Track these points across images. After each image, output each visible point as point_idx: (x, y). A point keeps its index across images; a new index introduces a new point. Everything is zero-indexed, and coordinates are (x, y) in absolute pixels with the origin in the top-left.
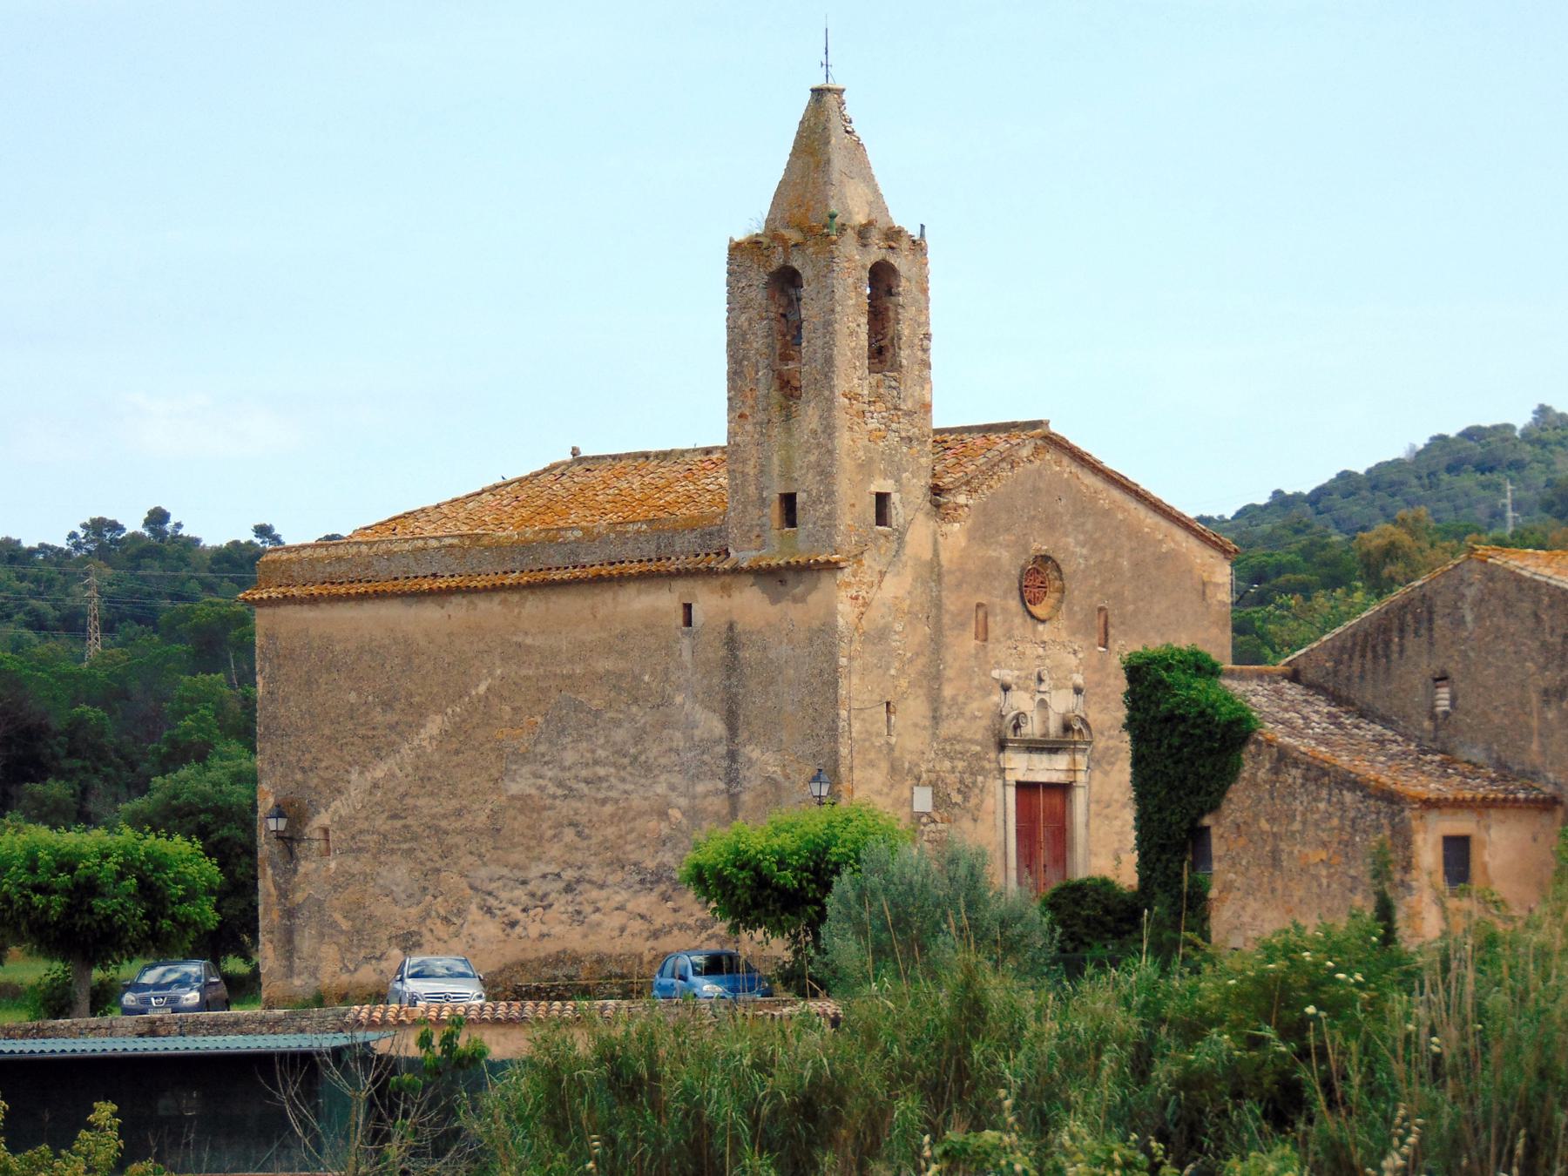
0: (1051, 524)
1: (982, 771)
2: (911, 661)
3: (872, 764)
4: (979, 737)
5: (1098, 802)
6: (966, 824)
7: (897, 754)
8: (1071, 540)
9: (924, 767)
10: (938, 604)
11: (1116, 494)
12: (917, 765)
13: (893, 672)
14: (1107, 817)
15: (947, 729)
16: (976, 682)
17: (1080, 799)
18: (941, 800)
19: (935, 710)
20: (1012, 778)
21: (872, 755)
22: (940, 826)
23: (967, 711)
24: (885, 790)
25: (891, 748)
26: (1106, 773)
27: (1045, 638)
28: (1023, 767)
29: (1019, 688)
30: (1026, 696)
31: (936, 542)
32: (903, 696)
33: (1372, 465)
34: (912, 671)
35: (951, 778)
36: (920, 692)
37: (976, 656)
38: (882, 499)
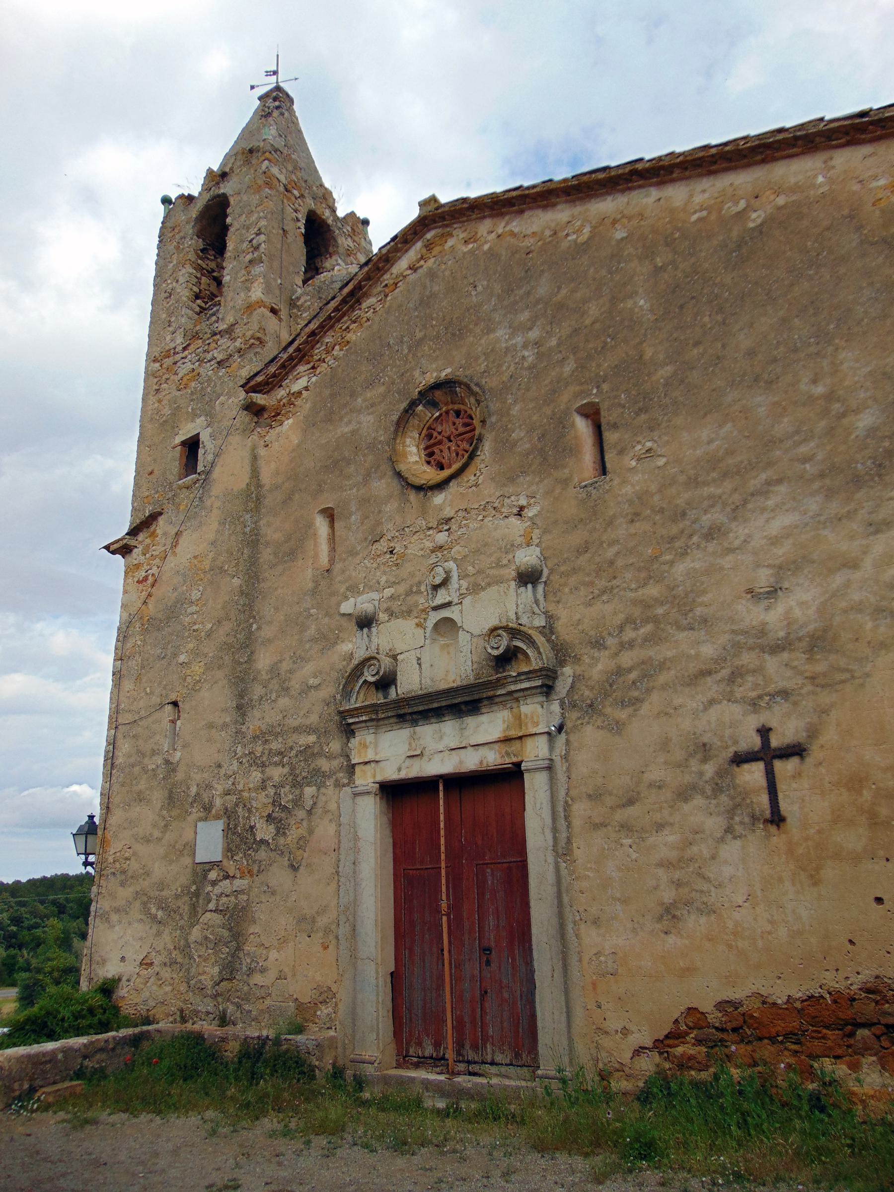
0: (455, 332)
1: (318, 777)
2: (209, 635)
3: (140, 798)
4: (314, 719)
5: (595, 797)
6: (279, 876)
7: (180, 776)
8: (501, 333)
9: (219, 788)
10: (254, 541)
11: (606, 206)
12: (209, 787)
13: (182, 658)
14: (626, 827)
15: (256, 721)
16: (312, 631)
17: (536, 788)
18: (239, 839)
19: (241, 696)
20: (366, 779)
21: (142, 785)
22: (238, 883)
23: (295, 685)
24: (157, 834)
25: (171, 767)
26: (618, 728)
27: (448, 512)
28: (392, 753)
29: (391, 614)
30: (407, 625)
31: (255, 458)
32: (196, 687)
33: (37, 876)
34: (210, 649)
35: (261, 800)
36: (220, 674)
37: (314, 592)
38: (192, 446)
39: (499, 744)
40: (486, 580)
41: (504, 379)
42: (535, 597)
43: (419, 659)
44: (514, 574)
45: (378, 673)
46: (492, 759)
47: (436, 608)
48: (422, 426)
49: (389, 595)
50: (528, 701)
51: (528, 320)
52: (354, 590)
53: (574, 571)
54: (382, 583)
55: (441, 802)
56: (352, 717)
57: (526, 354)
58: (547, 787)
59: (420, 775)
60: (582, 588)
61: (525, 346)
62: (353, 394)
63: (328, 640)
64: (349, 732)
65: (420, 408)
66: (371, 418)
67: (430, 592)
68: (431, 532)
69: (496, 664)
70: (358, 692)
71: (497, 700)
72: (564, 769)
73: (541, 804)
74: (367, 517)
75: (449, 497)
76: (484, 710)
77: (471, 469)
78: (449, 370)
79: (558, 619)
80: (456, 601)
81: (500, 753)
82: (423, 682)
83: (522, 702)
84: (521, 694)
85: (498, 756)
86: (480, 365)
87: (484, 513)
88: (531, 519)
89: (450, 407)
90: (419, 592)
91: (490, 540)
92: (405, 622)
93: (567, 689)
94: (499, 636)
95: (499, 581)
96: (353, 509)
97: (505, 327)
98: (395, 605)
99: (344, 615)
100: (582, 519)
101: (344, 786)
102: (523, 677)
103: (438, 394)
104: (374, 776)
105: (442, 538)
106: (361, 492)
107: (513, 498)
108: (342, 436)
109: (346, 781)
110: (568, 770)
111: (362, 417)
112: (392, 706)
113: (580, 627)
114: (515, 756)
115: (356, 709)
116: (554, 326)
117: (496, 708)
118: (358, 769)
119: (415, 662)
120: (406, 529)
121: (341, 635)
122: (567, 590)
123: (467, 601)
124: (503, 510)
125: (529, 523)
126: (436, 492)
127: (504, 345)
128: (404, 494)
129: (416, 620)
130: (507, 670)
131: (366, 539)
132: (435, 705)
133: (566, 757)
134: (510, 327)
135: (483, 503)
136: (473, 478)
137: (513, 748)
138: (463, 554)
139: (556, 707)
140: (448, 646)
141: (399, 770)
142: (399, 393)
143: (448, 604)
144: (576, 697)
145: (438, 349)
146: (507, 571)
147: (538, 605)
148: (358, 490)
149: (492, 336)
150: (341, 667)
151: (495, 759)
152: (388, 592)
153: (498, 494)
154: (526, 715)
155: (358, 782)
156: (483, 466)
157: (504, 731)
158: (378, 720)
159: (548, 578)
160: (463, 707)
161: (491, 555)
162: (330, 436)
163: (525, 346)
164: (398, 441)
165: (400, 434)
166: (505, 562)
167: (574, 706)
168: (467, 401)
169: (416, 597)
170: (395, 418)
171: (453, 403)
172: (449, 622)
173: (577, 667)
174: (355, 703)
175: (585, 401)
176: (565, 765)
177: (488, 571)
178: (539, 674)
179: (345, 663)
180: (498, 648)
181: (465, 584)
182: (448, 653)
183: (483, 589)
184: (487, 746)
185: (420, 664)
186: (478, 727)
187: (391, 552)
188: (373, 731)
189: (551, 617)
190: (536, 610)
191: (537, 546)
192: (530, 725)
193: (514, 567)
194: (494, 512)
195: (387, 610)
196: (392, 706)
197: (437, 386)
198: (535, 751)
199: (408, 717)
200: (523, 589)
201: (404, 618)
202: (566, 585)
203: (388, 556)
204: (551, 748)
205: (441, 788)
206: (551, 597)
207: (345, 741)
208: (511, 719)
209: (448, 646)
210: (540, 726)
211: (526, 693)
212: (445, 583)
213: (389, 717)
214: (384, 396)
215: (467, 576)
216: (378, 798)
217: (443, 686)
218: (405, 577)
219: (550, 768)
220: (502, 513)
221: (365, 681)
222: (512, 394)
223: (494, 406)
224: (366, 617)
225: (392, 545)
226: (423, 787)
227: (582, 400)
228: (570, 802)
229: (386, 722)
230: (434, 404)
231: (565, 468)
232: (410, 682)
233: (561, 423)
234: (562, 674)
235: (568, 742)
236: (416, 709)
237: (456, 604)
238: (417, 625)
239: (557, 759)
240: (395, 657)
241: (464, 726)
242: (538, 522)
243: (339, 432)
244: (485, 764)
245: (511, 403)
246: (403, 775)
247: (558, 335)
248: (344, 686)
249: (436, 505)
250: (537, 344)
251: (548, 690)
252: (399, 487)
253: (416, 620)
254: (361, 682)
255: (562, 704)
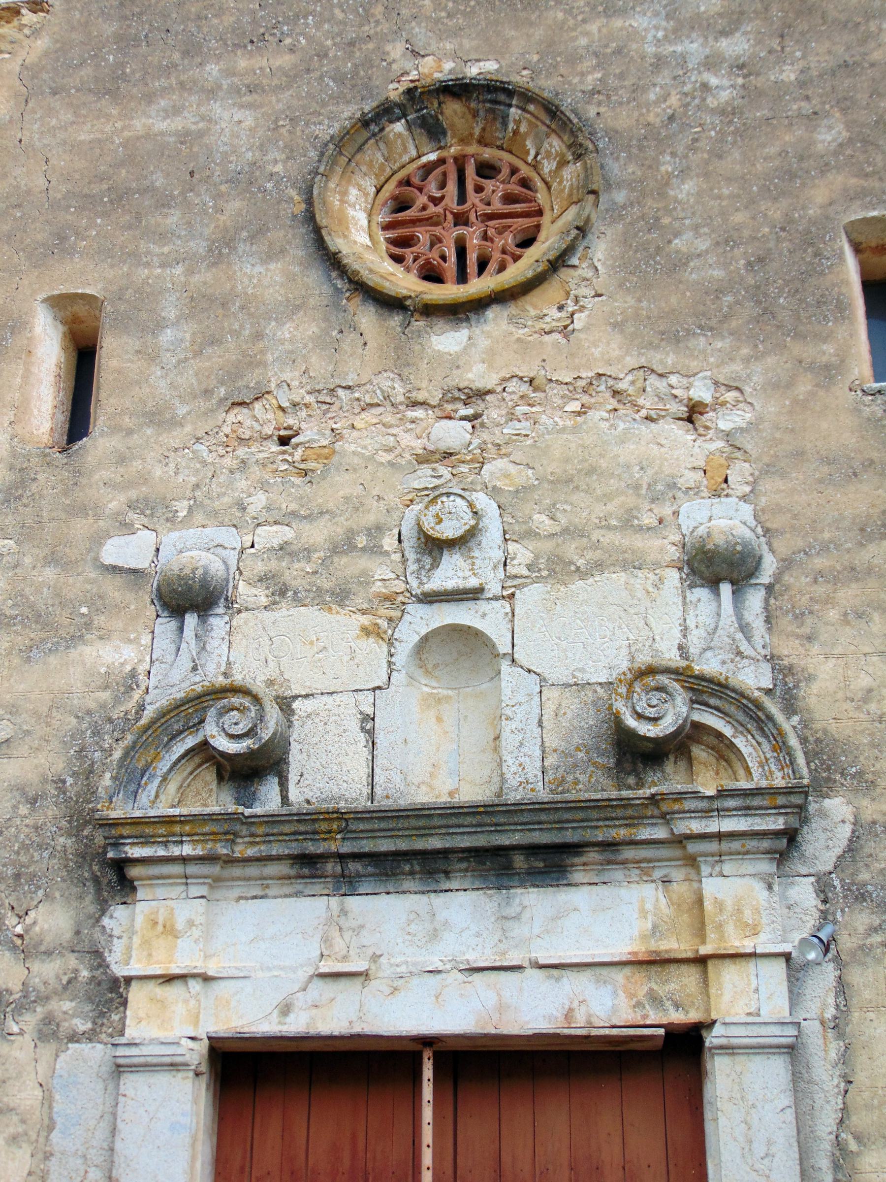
20: (173, 1026)
27: (477, 375)
28: (266, 962)
29: (281, 592)
39: (627, 971)
40: (589, 555)
41: (651, 118)
42: (739, 617)
43: (368, 718)
44: (674, 553)
45: (250, 733)
46: (606, 1008)
47: (430, 598)
48: (388, 172)
49: (276, 542)
50: (727, 868)
51: (720, 15)
52: (153, 509)
53: (853, 573)
54: (251, 510)
55: (427, 1114)
56: (146, 840)
57: (714, 81)
58: (786, 1100)
59: (357, 1029)
60: (876, 616)
61: (711, 63)
62: (192, 50)
63: (50, 628)
64: (117, 879)
65: (399, 127)
66: (248, 118)
67: (411, 556)
68: (419, 413)
69: (619, 763)
70: (165, 779)
71: (629, 853)
72: (833, 1055)
73: (769, 1143)
74: (214, 341)
75: (483, 343)
76: (578, 876)
77: (551, 291)
78: (490, 66)
79: (810, 678)
80: (494, 588)
81: (631, 996)
82: (379, 778)
83: (705, 870)
84: (713, 846)
85: (623, 1002)
86: (582, 74)
87: (585, 399)
88: (727, 436)
89: (472, 149)
90: (375, 550)
91: (603, 463)
92: (324, 618)
93: (838, 851)
94: (660, 689)
95: (632, 563)
96: (171, 313)
97: (656, 14)
98: (295, 573)
99: (115, 569)
100: (872, 462)
101: (74, 1038)
102: (731, 803)
103: (453, 110)
104: (196, 1020)
105: (453, 433)
106: (196, 279)
107: (673, 379)
108: (147, 136)
109: (82, 1025)
110: (846, 1058)
111: (216, 108)
112: (287, 829)
113: (873, 707)
114: (677, 1006)
115: (168, 821)
116: (790, 43)
117: (618, 874)
118: (136, 995)
119: (354, 725)
120: (340, 392)
121: (100, 620)
122: (833, 614)
123: (530, 597)
124: (641, 401)
125: (720, 444)
126: (440, 324)
127: (650, 49)
128: (337, 306)
129: (365, 620)
130: (635, 787)
131: (207, 393)
132: (435, 843)
133: (837, 1026)
134: (668, 17)
135: (587, 374)
136: (554, 313)
137: (672, 986)
138: (520, 481)
139: (804, 892)
140: (439, 701)
141: (286, 1009)
142: (340, 79)
143: (473, 594)
144: (864, 876)
145: (464, 14)
146: (657, 543)
147: (748, 639)
148: (190, 272)
149: (618, 23)
150: (92, 705)
151: (615, 1009)
152: (271, 536)
153: (631, 361)
154: (720, 905)
155: (131, 1032)
156: (583, 291)
157: (644, 937)
158: (230, 861)
159: (778, 577)
160: (519, 861)
161: (607, 498)
162: (108, 128)
163: (711, 63)
164: (332, 185)
165: (339, 170)
166: (648, 520)
167: (859, 896)
168: (529, 144)
169: (364, 562)
170: (327, 129)
171: (482, 142)
172: (467, 643)
173: (865, 802)
174: (158, 799)
175: (875, 213)
176: (834, 1049)
177: (596, 535)
178: (781, 800)
179: (105, 696)
180: (655, 720)
181: (522, 554)
182: (439, 719)
183: (581, 574)
184: (588, 973)
185: (371, 734)
186: (556, 918)
187: (284, 441)
188: (203, 890)
189: (790, 670)
190: (744, 647)
191: (744, 498)
192: (730, 929)
193: (677, 538)
194: (613, 403)
195: (264, 579)
196: (287, 829)
197: (458, 89)
198: (745, 1001)
199: (331, 867)
200: (702, 594)
201: (323, 605)
202: (828, 601)
203: (275, 448)
204: (795, 997)
205: (428, 1072)
206: (785, 622)
207: (92, 909)
208: (665, 909)
209: (439, 701)
210: (762, 937)
211: (725, 846)
212: (462, 542)
213: (270, 859)
214: (292, 78)
215: (531, 534)
216: (204, 1081)
217: (423, 797)
218: (331, 506)
219: (792, 1050)
220: (638, 408)
221: (205, 743)
222: (673, 154)
223: (619, 168)
224: (205, 583)
225: (291, 421)
226: (373, 1067)
227: (865, 207)
228: (853, 1146)
229: (253, 870)
230: (433, 130)
231: (825, 341)
232: (326, 771)
233: (812, 244)
234: (823, 814)
235: (842, 987)
236: (367, 846)
237: (495, 598)
238: (366, 631)
239: (812, 1028)
240: (285, 704)
241: (511, 911)
242: (748, 447)
243: (139, 124)
244: (580, 1019)
245: (669, 175)
246: (296, 1024)
247: (801, 64)
248: (126, 754)
249: (440, 354)
250: (740, 66)
251: (786, 845)
252: (326, 289)
253: (365, 620)
254: (190, 741)
255: (823, 889)
